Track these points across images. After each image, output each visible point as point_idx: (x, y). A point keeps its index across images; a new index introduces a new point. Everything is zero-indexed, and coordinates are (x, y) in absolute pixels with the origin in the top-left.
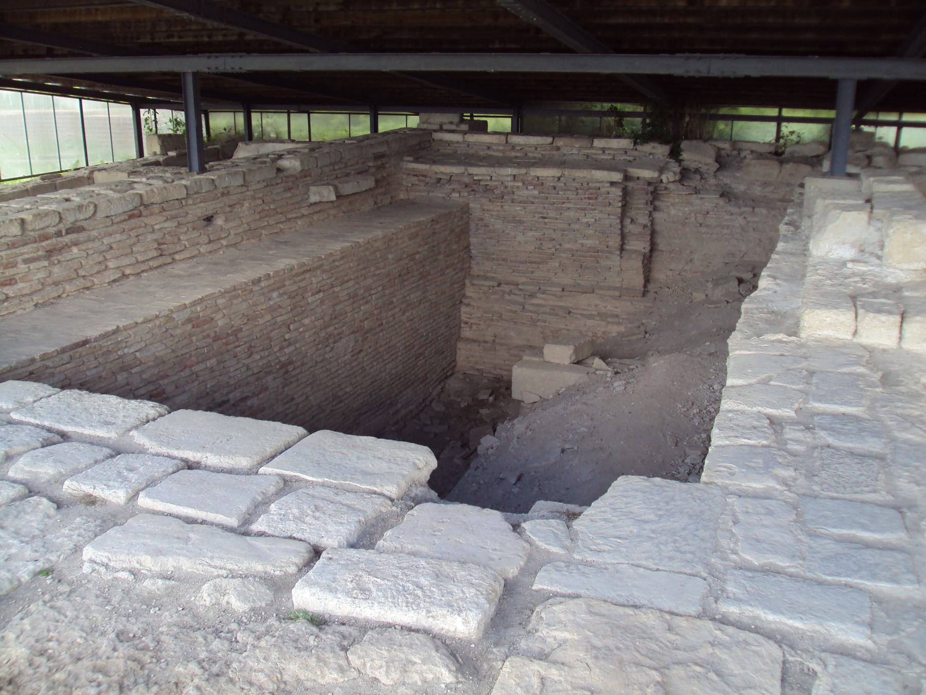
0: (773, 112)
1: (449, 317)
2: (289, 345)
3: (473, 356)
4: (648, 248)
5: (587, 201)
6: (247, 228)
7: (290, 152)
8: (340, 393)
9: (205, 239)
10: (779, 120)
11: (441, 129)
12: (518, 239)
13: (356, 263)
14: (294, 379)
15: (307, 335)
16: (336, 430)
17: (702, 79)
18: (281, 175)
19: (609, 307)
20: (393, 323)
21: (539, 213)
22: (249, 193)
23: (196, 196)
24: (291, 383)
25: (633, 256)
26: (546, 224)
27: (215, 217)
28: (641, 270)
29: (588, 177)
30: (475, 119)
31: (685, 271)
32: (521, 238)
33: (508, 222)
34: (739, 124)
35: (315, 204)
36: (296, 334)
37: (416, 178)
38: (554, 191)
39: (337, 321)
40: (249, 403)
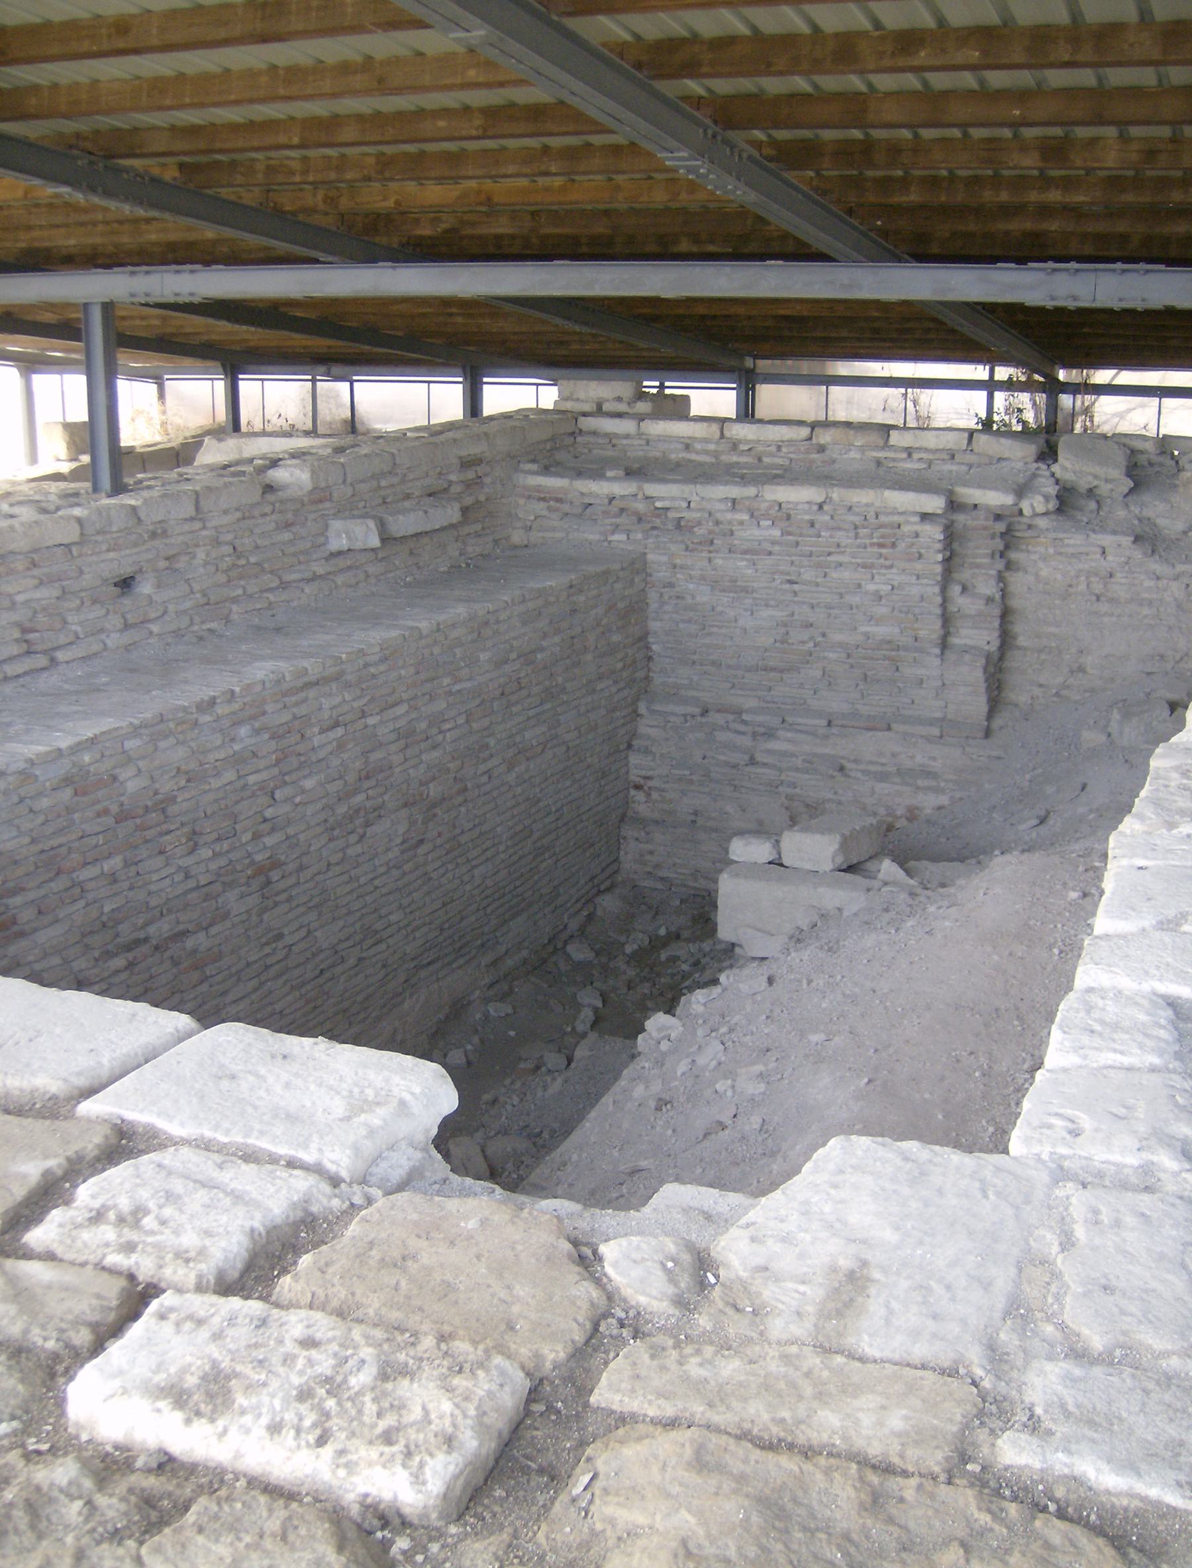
0: (979, 372)
1: (604, 775)
2: (273, 830)
3: (651, 853)
4: (996, 643)
5: (876, 549)
6: (203, 601)
7: (297, 455)
8: (378, 926)
9: (115, 621)
10: (990, 386)
11: (599, 411)
12: (741, 623)
13: (412, 670)
14: (283, 896)
15: (310, 810)
16: (256, 1023)
17: (1082, 311)
18: (270, 497)
19: (919, 759)
20: (488, 787)
21: (783, 573)
22: (204, 533)
23: (99, 538)
24: (276, 904)
25: (967, 657)
26: (795, 594)
27: (138, 578)
28: (982, 687)
29: (878, 504)
30: (667, 391)
31: (1068, 687)
32: (746, 621)
33: (723, 591)
34: (838, 392)
35: (340, 553)
36: (285, 808)
37: (542, 505)
38: (812, 531)
39: (372, 782)
40: (190, 943)
